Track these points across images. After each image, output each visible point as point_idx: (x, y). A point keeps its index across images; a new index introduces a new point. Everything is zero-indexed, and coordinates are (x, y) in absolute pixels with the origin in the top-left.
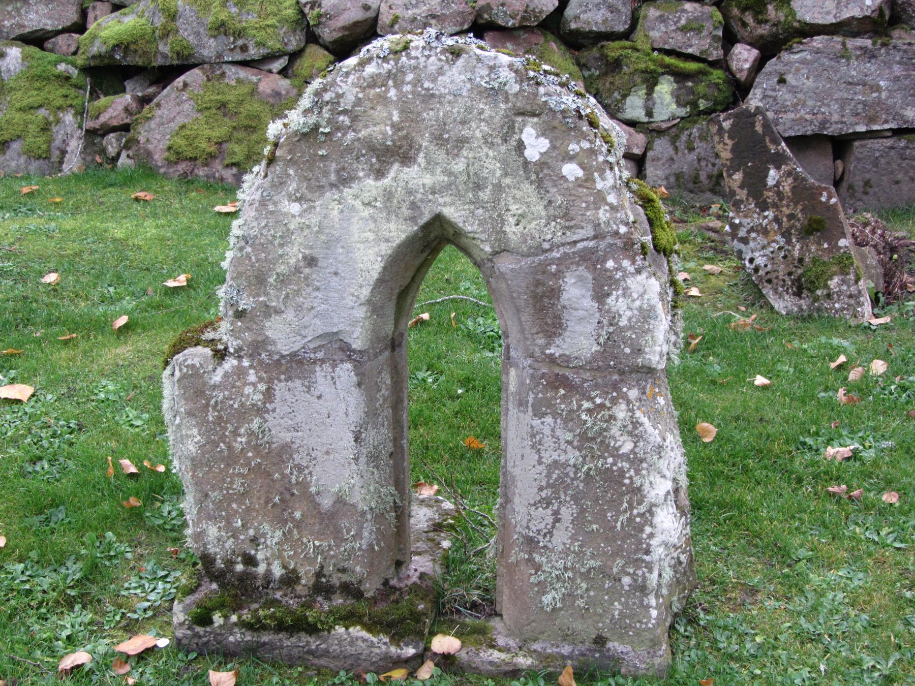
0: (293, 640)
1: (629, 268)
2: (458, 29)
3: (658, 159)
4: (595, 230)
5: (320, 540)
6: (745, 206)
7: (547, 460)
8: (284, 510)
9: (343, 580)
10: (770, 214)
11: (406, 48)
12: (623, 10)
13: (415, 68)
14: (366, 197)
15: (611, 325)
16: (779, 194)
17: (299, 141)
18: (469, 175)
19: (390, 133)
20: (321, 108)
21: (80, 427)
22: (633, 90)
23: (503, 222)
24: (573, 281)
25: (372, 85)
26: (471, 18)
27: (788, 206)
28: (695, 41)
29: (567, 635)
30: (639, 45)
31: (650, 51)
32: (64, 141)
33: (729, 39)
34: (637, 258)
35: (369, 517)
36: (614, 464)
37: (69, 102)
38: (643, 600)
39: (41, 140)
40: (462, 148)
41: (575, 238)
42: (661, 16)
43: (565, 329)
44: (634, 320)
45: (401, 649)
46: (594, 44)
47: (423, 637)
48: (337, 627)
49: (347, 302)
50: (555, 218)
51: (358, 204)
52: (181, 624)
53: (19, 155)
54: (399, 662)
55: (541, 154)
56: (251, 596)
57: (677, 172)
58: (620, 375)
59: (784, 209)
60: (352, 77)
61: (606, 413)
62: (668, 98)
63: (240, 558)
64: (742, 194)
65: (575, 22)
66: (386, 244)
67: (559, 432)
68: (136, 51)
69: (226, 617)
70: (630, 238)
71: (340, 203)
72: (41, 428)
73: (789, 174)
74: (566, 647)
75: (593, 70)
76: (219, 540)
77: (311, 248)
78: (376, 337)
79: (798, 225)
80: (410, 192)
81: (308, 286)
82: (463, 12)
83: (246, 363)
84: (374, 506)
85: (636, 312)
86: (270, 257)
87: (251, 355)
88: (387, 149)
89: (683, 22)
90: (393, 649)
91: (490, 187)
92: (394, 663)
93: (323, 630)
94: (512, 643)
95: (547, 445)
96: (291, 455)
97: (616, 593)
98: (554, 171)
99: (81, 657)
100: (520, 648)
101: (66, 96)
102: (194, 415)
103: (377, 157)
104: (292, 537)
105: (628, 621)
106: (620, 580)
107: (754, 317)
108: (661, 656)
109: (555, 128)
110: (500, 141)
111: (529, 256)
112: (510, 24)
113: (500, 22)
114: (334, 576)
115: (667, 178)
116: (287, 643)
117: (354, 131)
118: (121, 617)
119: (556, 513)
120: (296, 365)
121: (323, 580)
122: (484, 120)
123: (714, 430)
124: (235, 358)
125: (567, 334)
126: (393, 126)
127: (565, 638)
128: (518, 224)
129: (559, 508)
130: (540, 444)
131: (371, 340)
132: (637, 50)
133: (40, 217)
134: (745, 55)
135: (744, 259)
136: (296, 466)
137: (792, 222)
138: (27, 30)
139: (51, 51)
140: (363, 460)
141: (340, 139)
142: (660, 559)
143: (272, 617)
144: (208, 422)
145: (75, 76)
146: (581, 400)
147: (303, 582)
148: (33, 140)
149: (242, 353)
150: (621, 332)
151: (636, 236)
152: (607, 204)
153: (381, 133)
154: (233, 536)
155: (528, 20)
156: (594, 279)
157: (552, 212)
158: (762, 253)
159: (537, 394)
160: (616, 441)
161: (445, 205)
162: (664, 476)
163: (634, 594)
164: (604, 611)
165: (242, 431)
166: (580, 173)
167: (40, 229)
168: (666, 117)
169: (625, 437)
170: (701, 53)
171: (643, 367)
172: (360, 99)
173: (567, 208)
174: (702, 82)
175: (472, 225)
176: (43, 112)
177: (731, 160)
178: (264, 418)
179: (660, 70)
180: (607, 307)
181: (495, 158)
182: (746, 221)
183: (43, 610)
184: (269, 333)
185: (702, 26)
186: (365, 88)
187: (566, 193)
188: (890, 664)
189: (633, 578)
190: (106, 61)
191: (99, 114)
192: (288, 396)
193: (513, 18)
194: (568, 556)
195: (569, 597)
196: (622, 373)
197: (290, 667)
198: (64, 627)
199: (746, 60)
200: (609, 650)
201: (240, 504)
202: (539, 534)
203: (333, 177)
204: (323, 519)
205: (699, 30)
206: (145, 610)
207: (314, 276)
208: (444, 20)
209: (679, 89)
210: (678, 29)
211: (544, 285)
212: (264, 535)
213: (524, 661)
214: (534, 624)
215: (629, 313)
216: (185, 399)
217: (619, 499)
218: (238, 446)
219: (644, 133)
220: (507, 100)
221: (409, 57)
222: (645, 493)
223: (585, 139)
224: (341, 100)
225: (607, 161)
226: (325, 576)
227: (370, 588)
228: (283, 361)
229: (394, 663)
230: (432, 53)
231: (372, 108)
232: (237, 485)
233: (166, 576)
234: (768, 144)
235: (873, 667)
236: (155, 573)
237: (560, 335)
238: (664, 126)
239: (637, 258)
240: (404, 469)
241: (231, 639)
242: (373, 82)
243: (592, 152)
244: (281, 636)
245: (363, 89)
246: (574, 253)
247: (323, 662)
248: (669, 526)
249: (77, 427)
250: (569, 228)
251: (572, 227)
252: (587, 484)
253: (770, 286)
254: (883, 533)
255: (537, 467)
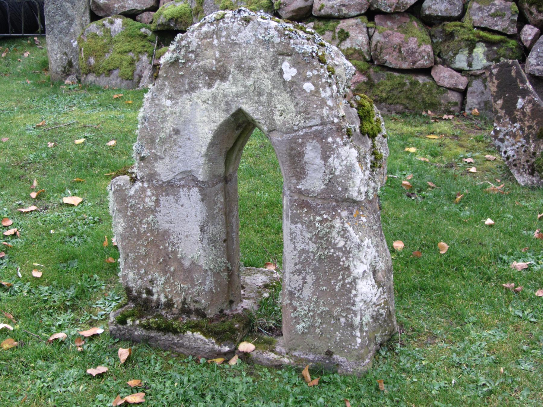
0: (166, 336)
1: (340, 142)
2: (358, 13)
3: (474, 92)
4: (321, 120)
5: (184, 284)
6: (503, 120)
7: (299, 249)
8: (166, 266)
9: (196, 307)
10: (517, 125)
11: (223, 18)
12: (457, 3)
13: (227, 28)
14: (204, 98)
15: (331, 174)
16: (524, 114)
17: (170, 66)
18: (255, 88)
19: (215, 63)
20: (181, 49)
21: (100, 220)
22: (460, 50)
23: (273, 114)
24: (311, 148)
25: (205, 38)
26: (366, 6)
27: (528, 121)
28: (499, 23)
29: (312, 349)
30: (465, 24)
31: (472, 28)
32: (141, 71)
33: (522, 21)
34: (344, 137)
35: (209, 273)
36: (334, 253)
37: (145, 50)
38: (352, 333)
39: (129, 69)
40: (251, 73)
41: (311, 124)
42: (479, 8)
43: (307, 175)
44: (343, 172)
45: (221, 347)
46: (440, 23)
47: (236, 342)
48: (188, 331)
49: (194, 152)
50: (300, 113)
51: (199, 101)
52: (112, 323)
53: (117, 77)
54: (219, 354)
55: (292, 77)
56: (149, 312)
57: (485, 100)
58: (337, 202)
59: (526, 122)
60: (195, 33)
61: (328, 223)
62: (481, 56)
63: (144, 291)
64: (502, 113)
65: (429, 10)
66: (214, 124)
67: (304, 233)
68: (181, 22)
69: (134, 321)
70: (340, 126)
71: (190, 101)
72: (80, 220)
73: (530, 101)
74: (311, 355)
75: (438, 39)
76: (134, 280)
77: (177, 124)
78: (213, 175)
79: (534, 132)
80: (225, 96)
81: (176, 145)
82: (361, 3)
83: (146, 185)
84: (212, 268)
85: (344, 167)
86: (157, 128)
87: (148, 181)
88: (214, 72)
89: (493, 11)
90: (216, 347)
91: (266, 94)
92: (218, 355)
93: (181, 332)
94: (284, 350)
95: (298, 240)
96: (169, 236)
97: (337, 326)
98: (299, 87)
99: (61, 335)
100: (287, 354)
101: (144, 46)
102: (121, 212)
103: (209, 77)
104: (170, 281)
105: (344, 344)
106: (339, 319)
107: (502, 185)
108: (363, 366)
109: (299, 62)
110: (271, 70)
111: (287, 133)
112: (388, 10)
113: (383, 9)
114: (191, 304)
115: (479, 104)
116: (163, 338)
117: (197, 62)
118: (90, 318)
119: (304, 278)
120: (169, 188)
121: (186, 306)
122: (262, 57)
123: (447, 247)
124: (141, 182)
125: (308, 178)
126: (216, 60)
127: (310, 350)
128: (281, 116)
129: (306, 276)
130: (295, 239)
131: (210, 176)
132: (464, 27)
133: (118, 111)
134: (530, 31)
135: (501, 152)
136: (171, 242)
137: (531, 130)
138: (127, 9)
139: (140, 21)
140: (205, 241)
141: (190, 66)
142: (361, 310)
143: (155, 323)
144: (128, 216)
145: (150, 35)
146: (315, 215)
147: (176, 306)
148: (125, 69)
149: (144, 180)
150: (336, 178)
151: (343, 124)
152: (327, 106)
153: (210, 63)
154: (141, 278)
155: (399, 8)
156: (321, 148)
157: (298, 109)
158: (511, 148)
159: (293, 211)
160: (335, 240)
161: (243, 103)
162: (362, 262)
163: (347, 328)
164: (331, 336)
165: (144, 221)
166: (313, 88)
167: (116, 117)
168: (480, 68)
169: (339, 238)
170: (503, 30)
171: (348, 199)
172: (199, 45)
173: (306, 107)
174: (502, 47)
175: (257, 115)
176: (131, 55)
177: (496, 92)
178: (155, 215)
179: (477, 39)
180: (328, 164)
181: (268, 78)
182: (503, 129)
183: (51, 311)
184: (157, 170)
185: (505, 14)
186: (202, 39)
187: (306, 99)
188: (496, 384)
189: (346, 319)
190: (166, 27)
191: (160, 56)
192: (167, 204)
193: (390, 7)
194: (311, 303)
195: (312, 326)
196: (337, 201)
197: (165, 351)
198: (59, 320)
199: (530, 35)
200: (334, 359)
201: (145, 261)
202: (295, 289)
203: (187, 87)
204: (185, 273)
205: (502, 16)
206: (102, 315)
207: (178, 140)
208: (350, 8)
209: (489, 51)
210: (489, 15)
211: (295, 150)
212: (156, 279)
213: (286, 360)
214: (294, 341)
215: (340, 168)
216: (117, 203)
217: (338, 273)
218: (142, 230)
219: (467, 77)
220: (274, 47)
221: (224, 22)
222: (352, 271)
223: (315, 69)
224: (190, 45)
225: (327, 82)
226: (187, 304)
227: (211, 313)
228: (164, 185)
229: (218, 355)
230: (236, 20)
231: (206, 50)
232: (142, 251)
233: (118, 300)
234: (519, 83)
235: (484, 385)
236: (114, 297)
237: (304, 178)
238: (479, 72)
239: (344, 137)
240: (234, 249)
241: (136, 333)
242: (206, 36)
243: (319, 77)
244: (160, 334)
245: (201, 40)
246: (310, 133)
247: (181, 350)
248: (367, 291)
249: (98, 221)
250: (308, 118)
251: (309, 118)
252: (320, 263)
253: (515, 168)
254: (526, 313)
255: (293, 251)
